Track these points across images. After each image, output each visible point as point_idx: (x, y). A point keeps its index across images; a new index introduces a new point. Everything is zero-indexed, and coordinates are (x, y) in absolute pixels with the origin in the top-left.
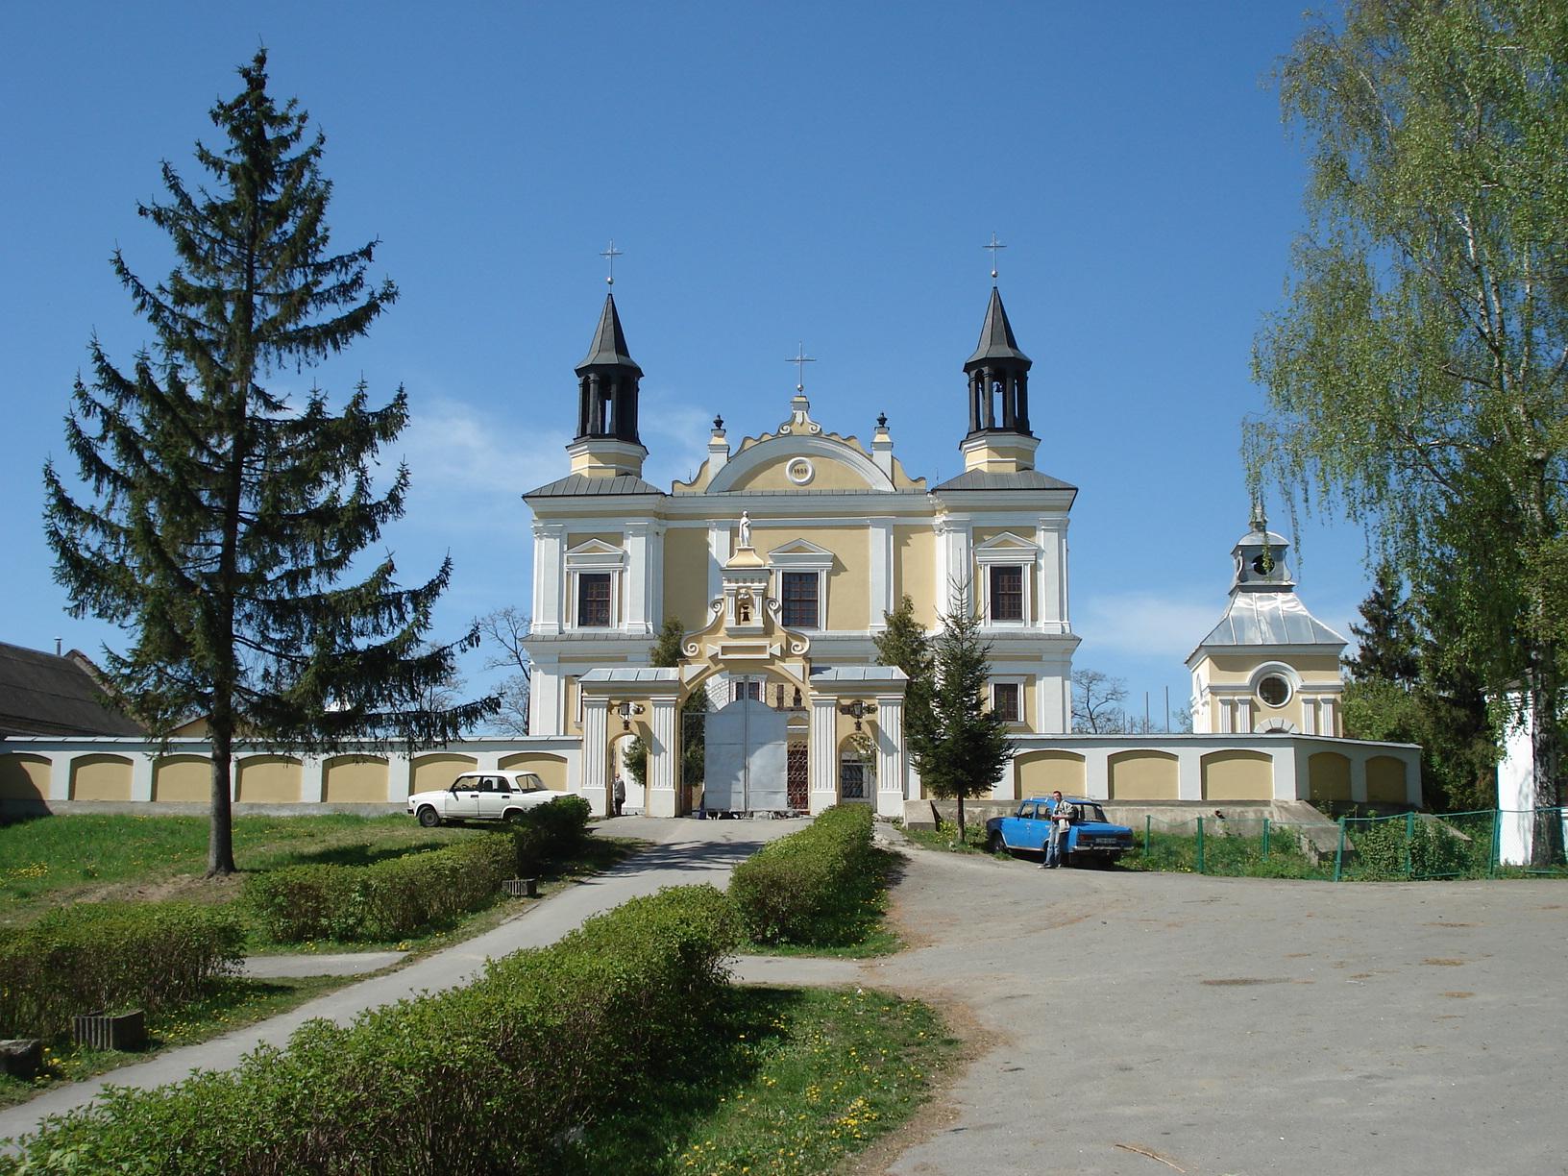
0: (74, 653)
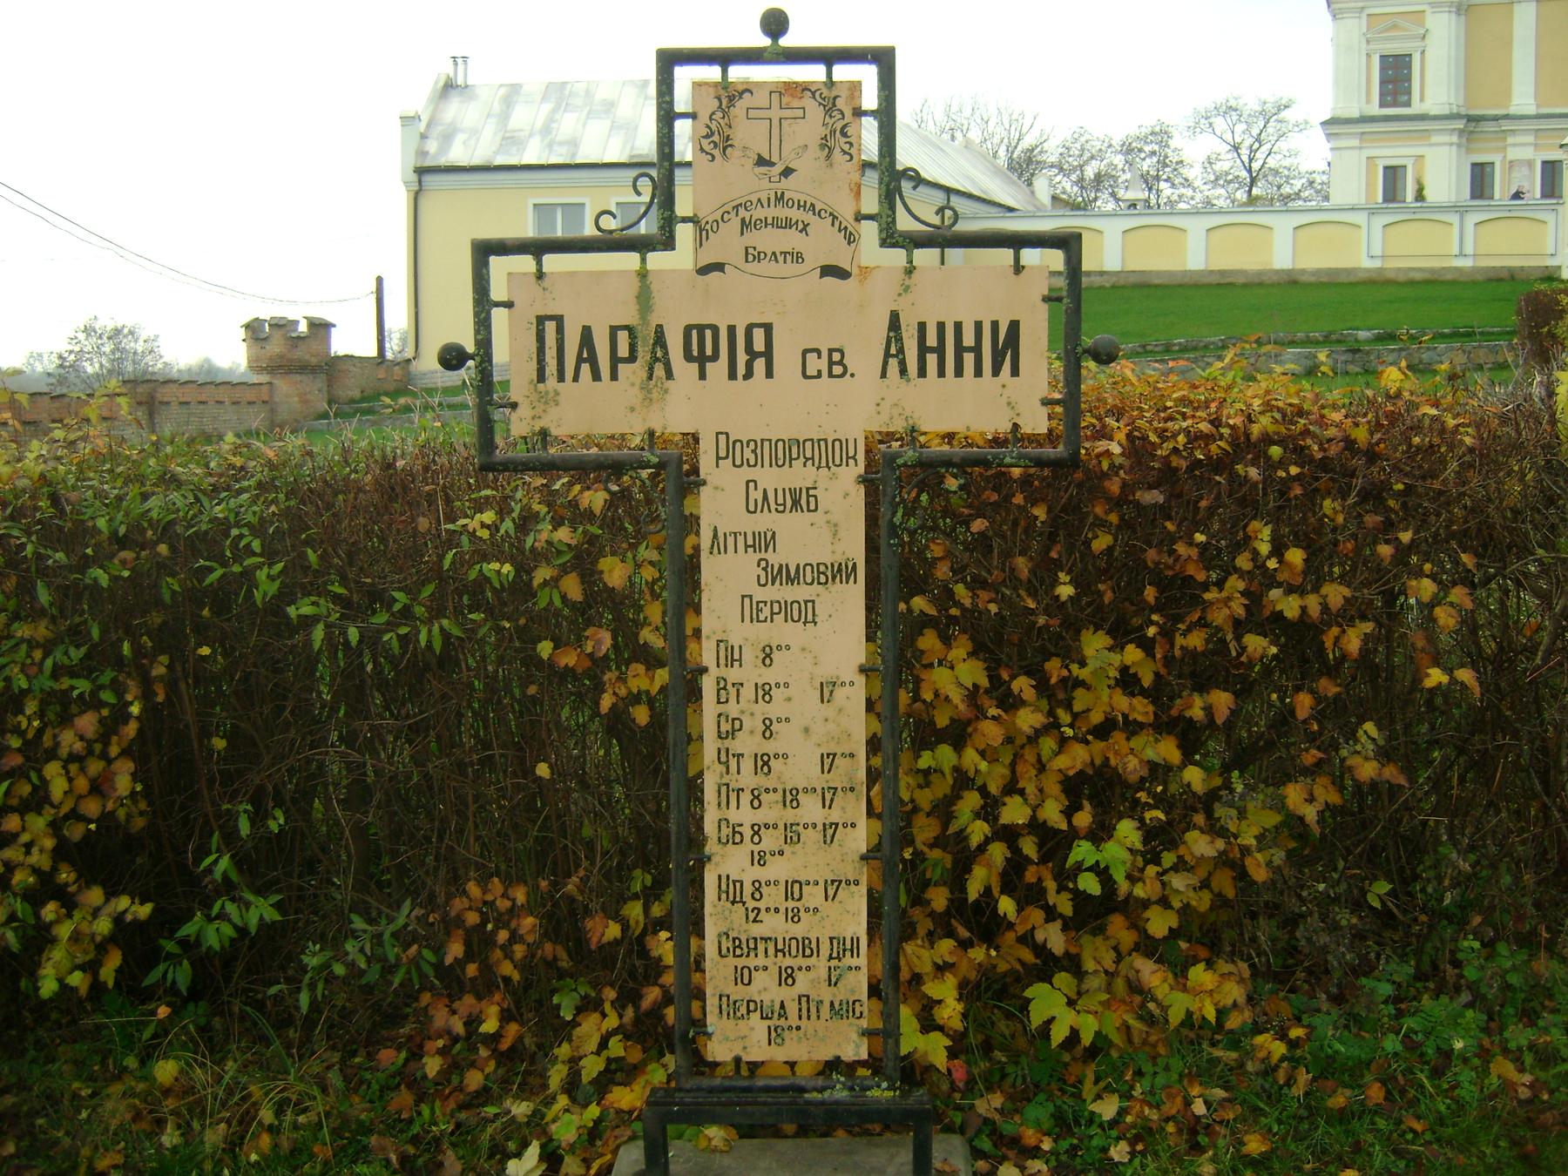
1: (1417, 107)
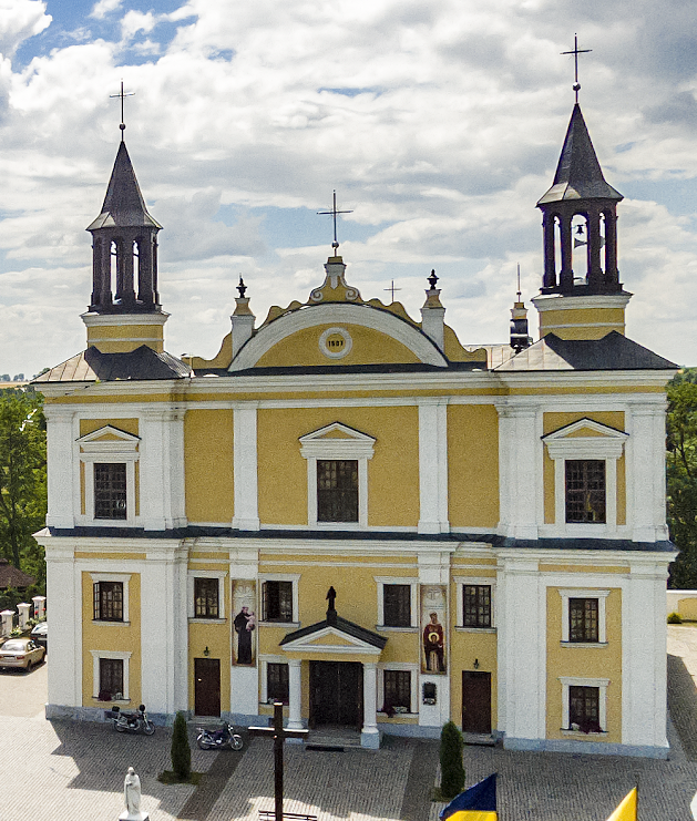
0: (145, 14)
1: (131, 521)
